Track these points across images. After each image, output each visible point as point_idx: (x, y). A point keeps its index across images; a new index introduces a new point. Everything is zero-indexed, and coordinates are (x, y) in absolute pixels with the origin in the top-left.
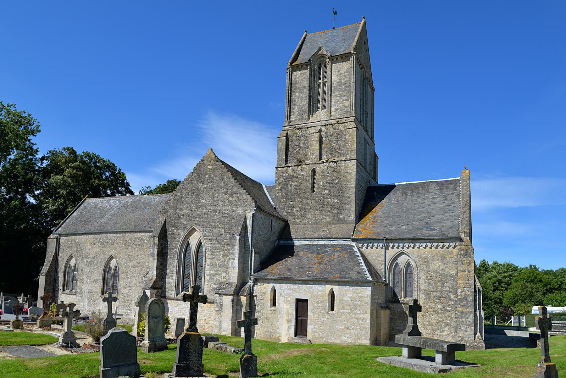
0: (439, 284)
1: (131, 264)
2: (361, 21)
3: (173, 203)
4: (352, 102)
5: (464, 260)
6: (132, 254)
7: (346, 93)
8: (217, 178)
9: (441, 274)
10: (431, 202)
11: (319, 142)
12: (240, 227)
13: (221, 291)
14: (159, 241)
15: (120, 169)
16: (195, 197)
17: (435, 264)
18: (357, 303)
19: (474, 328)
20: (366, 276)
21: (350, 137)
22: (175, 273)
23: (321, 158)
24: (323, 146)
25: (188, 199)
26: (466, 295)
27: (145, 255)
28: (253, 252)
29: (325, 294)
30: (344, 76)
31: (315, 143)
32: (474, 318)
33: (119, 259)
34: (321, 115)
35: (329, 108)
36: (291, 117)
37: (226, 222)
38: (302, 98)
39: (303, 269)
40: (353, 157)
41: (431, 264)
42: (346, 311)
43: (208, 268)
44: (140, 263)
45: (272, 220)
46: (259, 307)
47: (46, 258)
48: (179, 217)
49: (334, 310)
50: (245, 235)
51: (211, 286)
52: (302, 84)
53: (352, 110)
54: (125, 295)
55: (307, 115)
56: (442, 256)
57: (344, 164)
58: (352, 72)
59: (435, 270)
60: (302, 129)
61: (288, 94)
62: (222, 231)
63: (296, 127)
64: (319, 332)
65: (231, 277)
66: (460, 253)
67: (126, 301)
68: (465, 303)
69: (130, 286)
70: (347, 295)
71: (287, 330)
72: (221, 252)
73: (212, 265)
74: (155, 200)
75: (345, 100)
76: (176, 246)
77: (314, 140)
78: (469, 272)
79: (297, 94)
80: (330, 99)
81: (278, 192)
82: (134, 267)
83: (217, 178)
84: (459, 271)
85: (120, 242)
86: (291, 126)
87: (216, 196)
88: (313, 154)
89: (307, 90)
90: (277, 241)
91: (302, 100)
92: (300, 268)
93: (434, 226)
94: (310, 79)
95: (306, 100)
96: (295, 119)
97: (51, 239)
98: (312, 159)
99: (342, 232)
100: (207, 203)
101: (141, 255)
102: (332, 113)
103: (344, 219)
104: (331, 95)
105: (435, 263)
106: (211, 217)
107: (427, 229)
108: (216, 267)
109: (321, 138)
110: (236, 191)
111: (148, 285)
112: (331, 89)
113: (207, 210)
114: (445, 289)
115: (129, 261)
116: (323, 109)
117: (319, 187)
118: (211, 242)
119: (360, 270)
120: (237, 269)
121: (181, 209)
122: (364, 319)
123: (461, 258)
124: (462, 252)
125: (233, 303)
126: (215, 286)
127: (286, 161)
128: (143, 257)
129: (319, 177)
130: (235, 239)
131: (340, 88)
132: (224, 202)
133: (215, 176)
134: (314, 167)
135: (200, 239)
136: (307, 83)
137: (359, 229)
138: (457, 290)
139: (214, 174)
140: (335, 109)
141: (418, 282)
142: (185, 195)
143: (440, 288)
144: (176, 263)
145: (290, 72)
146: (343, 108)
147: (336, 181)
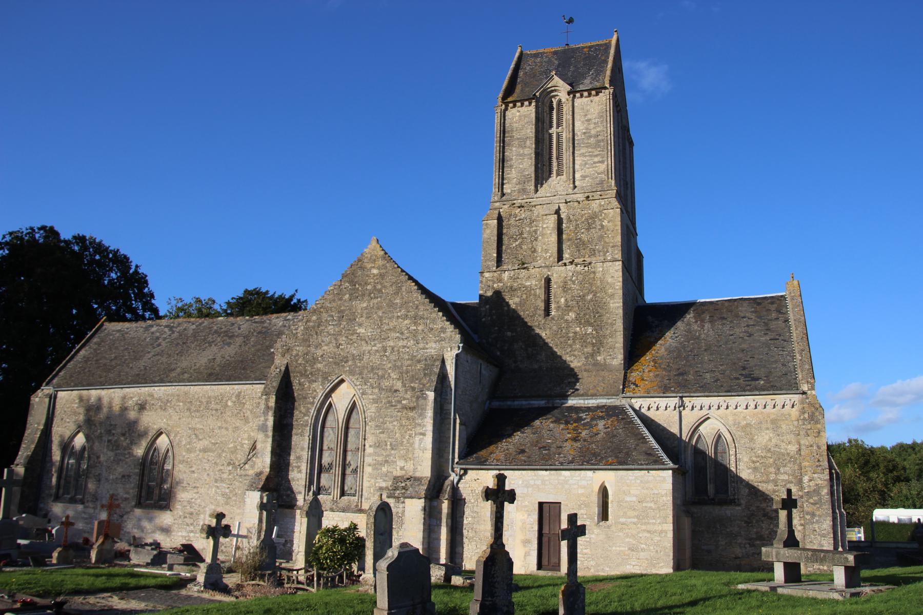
0: (772, 470)
1: (200, 445)
2: (612, 37)
3: (303, 335)
4: (610, 166)
5: (809, 427)
6: (201, 427)
7: (599, 151)
8: (387, 291)
9: (774, 453)
10: (744, 332)
11: (556, 231)
12: (434, 378)
13: (398, 492)
14: (276, 402)
15: (137, 266)
16: (345, 323)
17: (763, 436)
18: (649, 505)
19: (834, 540)
20: (662, 459)
21: (610, 224)
22: (305, 461)
23: (560, 258)
24: (564, 236)
25: (332, 327)
26: (817, 485)
27: (227, 429)
28: (458, 421)
29: (592, 491)
30: (595, 123)
31: (549, 232)
32: (831, 523)
33: (176, 436)
34: (556, 184)
35: (571, 174)
36: (504, 186)
37: (405, 368)
38: (523, 155)
39: (546, 450)
40: (616, 256)
41: (756, 437)
42: (629, 520)
43: (370, 452)
44: (217, 443)
45: (481, 364)
46: (470, 519)
47: (26, 435)
48: (315, 360)
49: (607, 520)
50: (442, 392)
51: (377, 485)
52: (523, 132)
53: (610, 180)
54: (185, 504)
55: (533, 184)
56: (774, 422)
57: (601, 269)
58: (608, 118)
59: (764, 446)
60: (526, 208)
61: (498, 148)
62: (399, 385)
63: (514, 204)
64: (583, 559)
65: (419, 467)
66: (802, 417)
67: (188, 516)
68: (816, 498)
69: (195, 487)
70: (632, 492)
71: (523, 559)
72: (395, 423)
73: (378, 446)
74: (242, 327)
75: (597, 162)
76: (308, 410)
77: (547, 227)
78: (819, 447)
79: (514, 149)
80: (571, 160)
81: (485, 315)
82: (205, 450)
83: (387, 291)
84: (803, 447)
85: (178, 404)
86: (505, 203)
87: (385, 323)
88: (546, 251)
89: (532, 144)
90: (488, 402)
91: (524, 159)
92: (541, 448)
93: (756, 373)
94: (536, 125)
95: (531, 159)
96: (512, 191)
97: (37, 399)
98: (545, 258)
99: (602, 384)
100: (369, 334)
101: (220, 428)
102: (577, 183)
103: (605, 363)
104: (573, 153)
105: (763, 434)
106: (375, 360)
107: (745, 378)
108: (387, 449)
109: (560, 222)
110: (423, 315)
111: (255, 483)
112: (574, 144)
113: (370, 348)
114: (782, 477)
115: (195, 440)
116: (558, 175)
117: (559, 307)
118: (377, 405)
119: (649, 449)
120: (431, 452)
121: (318, 346)
122: (661, 532)
123: (804, 424)
124: (806, 415)
125: (424, 514)
126: (384, 485)
127: (499, 261)
128: (224, 432)
129: (559, 291)
130: (425, 399)
131: (588, 143)
132: (402, 333)
133: (385, 287)
134: (549, 273)
135: (354, 398)
136: (531, 132)
137: (631, 379)
138: (802, 479)
139: (381, 284)
140: (581, 176)
141: (736, 467)
142: (326, 320)
143: (772, 477)
144: (307, 444)
145: (501, 112)
146: (594, 174)
147: (589, 298)
